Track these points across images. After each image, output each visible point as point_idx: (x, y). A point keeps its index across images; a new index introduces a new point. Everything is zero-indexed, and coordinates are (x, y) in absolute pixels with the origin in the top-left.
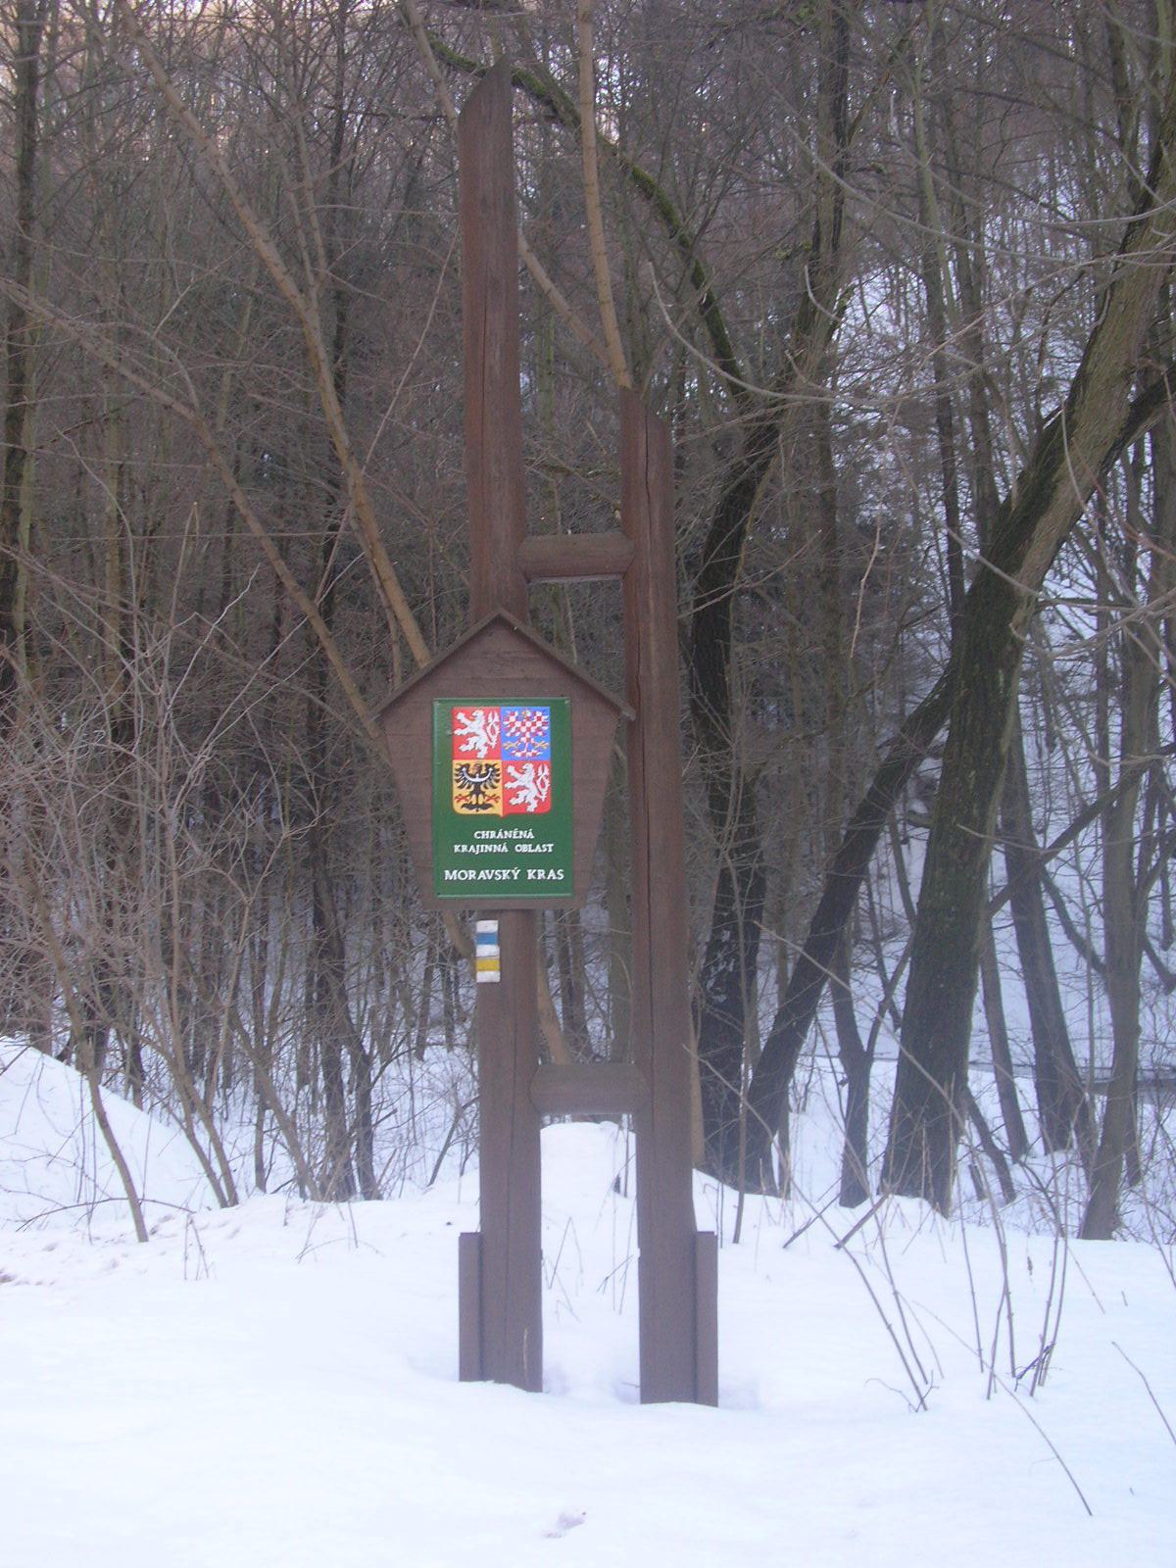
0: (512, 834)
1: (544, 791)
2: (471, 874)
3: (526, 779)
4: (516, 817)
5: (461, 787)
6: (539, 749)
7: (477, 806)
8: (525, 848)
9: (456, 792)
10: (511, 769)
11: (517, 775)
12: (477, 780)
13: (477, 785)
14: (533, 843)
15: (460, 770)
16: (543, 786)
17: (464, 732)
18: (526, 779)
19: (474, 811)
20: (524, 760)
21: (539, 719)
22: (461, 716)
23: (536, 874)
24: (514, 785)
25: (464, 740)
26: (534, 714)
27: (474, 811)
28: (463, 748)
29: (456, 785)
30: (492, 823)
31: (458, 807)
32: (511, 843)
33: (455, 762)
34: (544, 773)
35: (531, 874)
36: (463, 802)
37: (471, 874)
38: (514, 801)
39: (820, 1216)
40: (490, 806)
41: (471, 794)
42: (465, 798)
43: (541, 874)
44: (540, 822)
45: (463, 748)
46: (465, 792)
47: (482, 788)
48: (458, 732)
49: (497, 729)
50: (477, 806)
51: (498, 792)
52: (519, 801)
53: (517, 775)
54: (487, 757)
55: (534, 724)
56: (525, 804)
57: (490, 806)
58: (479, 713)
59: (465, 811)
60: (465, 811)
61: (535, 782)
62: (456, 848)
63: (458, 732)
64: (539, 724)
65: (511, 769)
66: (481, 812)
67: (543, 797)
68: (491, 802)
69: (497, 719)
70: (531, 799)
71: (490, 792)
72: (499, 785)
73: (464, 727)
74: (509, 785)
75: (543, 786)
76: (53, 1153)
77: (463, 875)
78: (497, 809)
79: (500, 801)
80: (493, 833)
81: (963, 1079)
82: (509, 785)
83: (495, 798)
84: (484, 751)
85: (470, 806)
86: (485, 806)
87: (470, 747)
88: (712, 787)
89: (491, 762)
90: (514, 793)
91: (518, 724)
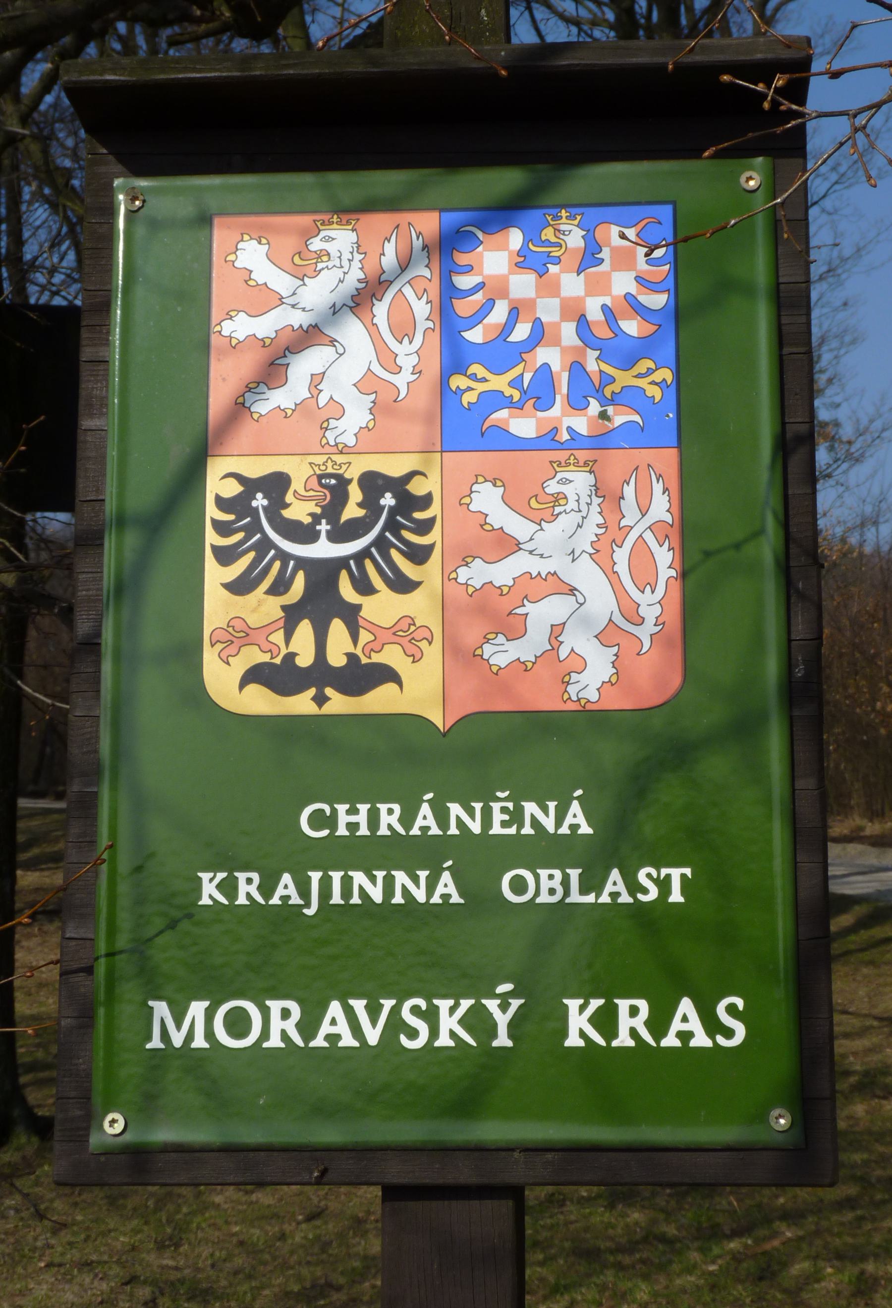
0: (488, 818)
2: (278, 1023)
4: (506, 743)
7: (321, 676)
9: (217, 606)
11: (518, 527)
12: (324, 549)
13: (323, 574)
14: (594, 859)
15: (235, 506)
19: (302, 704)
27: (302, 704)
29: (215, 575)
30: (403, 756)
31: (222, 679)
32: (479, 860)
35: (579, 1023)
37: (278, 1023)
38: (501, 654)
40: (388, 675)
44: (638, 769)
47: (347, 591)
50: (321, 676)
53: (518, 527)
57: (388, 675)
59: (259, 701)
60: (259, 701)
66: (338, 703)
68: (391, 656)
71: (382, 607)
74: (476, 574)
76: (680, 245)
77: (238, 1024)
78: (420, 690)
79: (433, 653)
80: (390, 818)
81: (24, 1100)
83: (406, 632)
85: (279, 677)
86: (361, 677)
90: (500, 614)
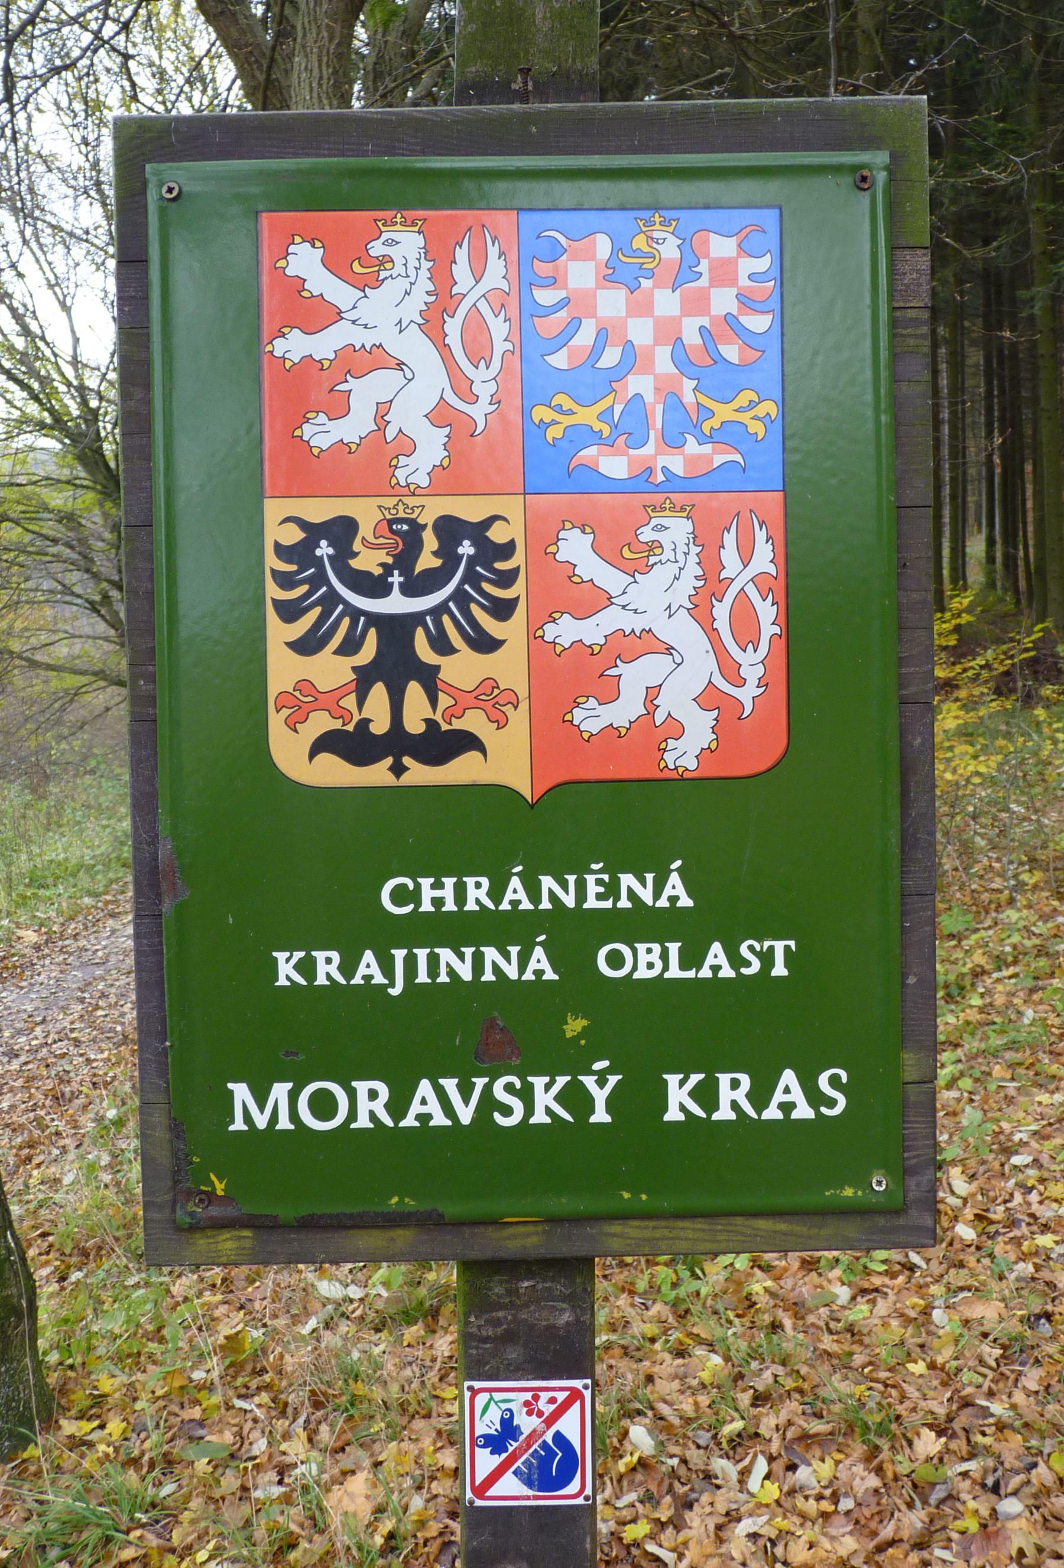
1: (752, 664)
2: (368, 1102)
3: (656, 598)
4: (611, 809)
5: (307, 646)
6: (725, 436)
7: (397, 744)
8: (647, 961)
9: (284, 669)
10: (576, 548)
11: (610, 579)
12: (396, 604)
13: (396, 631)
14: (690, 932)
16: (747, 637)
17: (323, 345)
18: (656, 598)
20: (650, 492)
21: (724, 272)
22: (305, 261)
23: (307, 967)
24: (592, 631)
25: (320, 388)
26: (692, 253)
27: (379, 774)
28: (322, 433)
29: (279, 633)
31: (290, 751)
32: (574, 935)
33: (274, 509)
34: (754, 563)
35: (679, 1097)
36: (321, 723)
37: (368, 1102)
38: (592, 717)
39: (525, 494)
40: (469, 742)
41: (364, 679)
42: (329, 701)
43: (327, 966)
45: (322, 433)
46: (331, 670)
48: (293, 346)
49: (498, 328)
50: (397, 744)
51: (509, 666)
52: (624, 711)
53: (610, 579)
54: (448, 478)
55: (697, 304)
56: (654, 730)
57: (469, 742)
58: (403, 244)
59: (334, 772)
61: (701, 610)
62: (287, 969)
63: (293, 346)
64: (724, 301)
65: (576, 548)
66: (418, 773)
67: (747, 695)
68: (473, 722)
69: (496, 272)
70: (679, 701)
71: (461, 668)
72: (511, 631)
73: (318, 315)
74: (565, 631)
75: (747, 637)
78: (506, 760)
79: (519, 719)
80: (478, 892)
82: (565, 631)
83: (491, 698)
84: (430, 449)
85: (355, 745)
86: (443, 745)
87: (354, 427)
88: (860, 1333)
89: (471, 510)
90: (593, 672)
91: (612, 303)
